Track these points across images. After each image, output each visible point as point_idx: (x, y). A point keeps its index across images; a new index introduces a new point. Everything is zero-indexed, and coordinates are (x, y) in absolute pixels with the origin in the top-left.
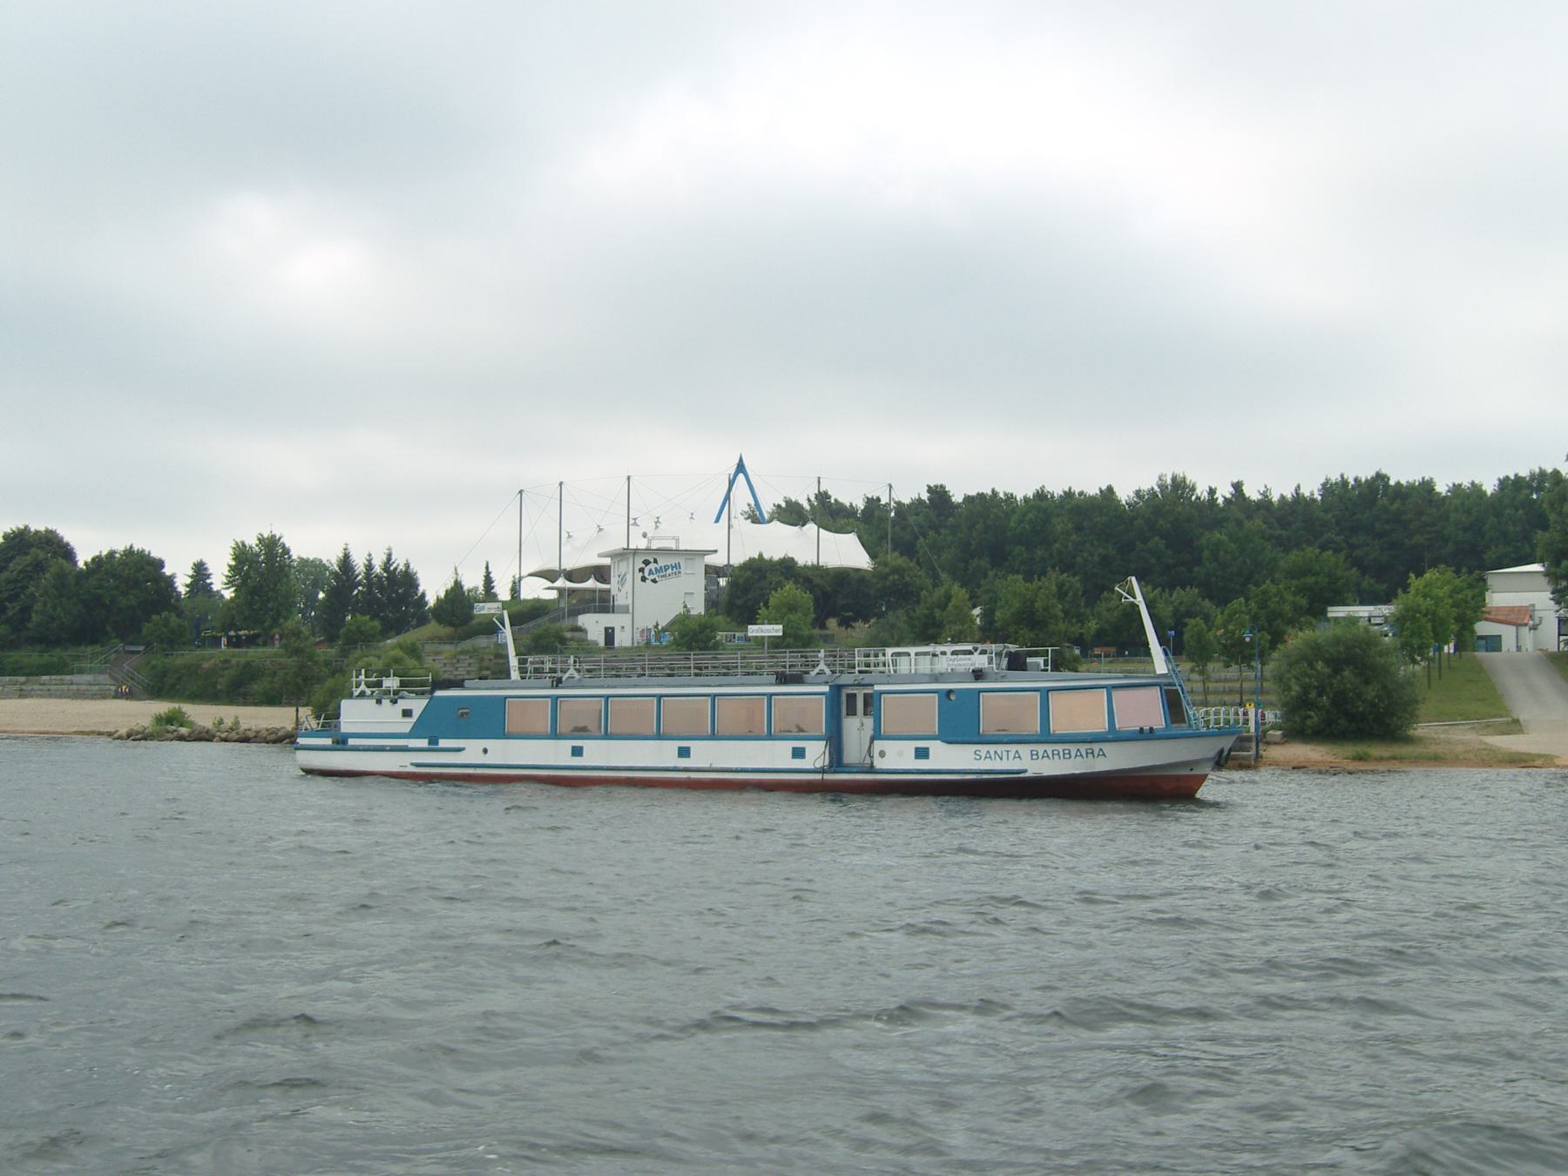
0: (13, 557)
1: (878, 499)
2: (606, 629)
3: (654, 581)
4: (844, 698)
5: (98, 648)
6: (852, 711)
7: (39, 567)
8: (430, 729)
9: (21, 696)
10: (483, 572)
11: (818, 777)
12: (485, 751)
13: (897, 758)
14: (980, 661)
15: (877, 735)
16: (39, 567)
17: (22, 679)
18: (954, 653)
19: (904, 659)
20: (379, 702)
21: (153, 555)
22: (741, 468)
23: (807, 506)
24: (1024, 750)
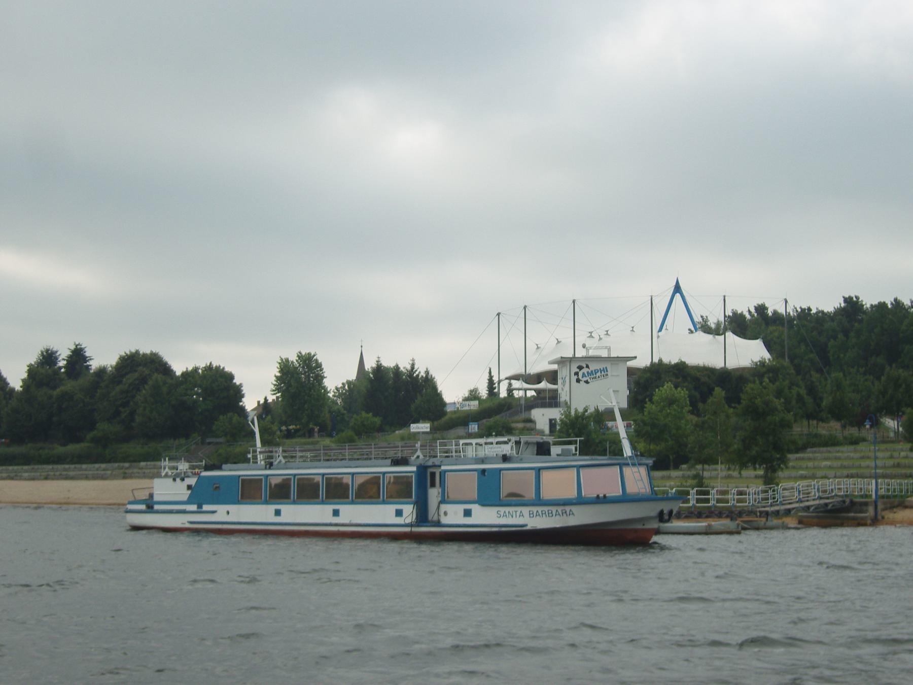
0: (127, 374)
1: (809, 309)
2: (551, 420)
3: (587, 382)
4: (429, 474)
5: (183, 441)
6: (433, 485)
7: (144, 380)
8: (201, 495)
9: (125, 478)
10: (487, 376)
11: (408, 529)
12: (228, 513)
13: (453, 516)
14: (507, 449)
15: (443, 501)
16: (144, 380)
17: (127, 465)
18: (497, 443)
19: (470, 448)
20: (174, 480)
21: (226, 369)
22: (677, 289)
23: (748, 317)
24: (525, 510)
